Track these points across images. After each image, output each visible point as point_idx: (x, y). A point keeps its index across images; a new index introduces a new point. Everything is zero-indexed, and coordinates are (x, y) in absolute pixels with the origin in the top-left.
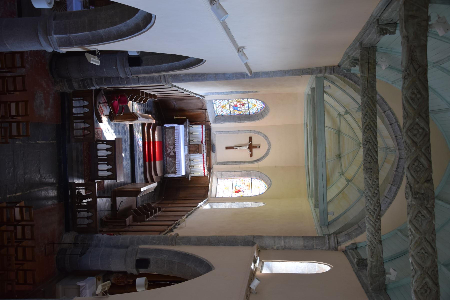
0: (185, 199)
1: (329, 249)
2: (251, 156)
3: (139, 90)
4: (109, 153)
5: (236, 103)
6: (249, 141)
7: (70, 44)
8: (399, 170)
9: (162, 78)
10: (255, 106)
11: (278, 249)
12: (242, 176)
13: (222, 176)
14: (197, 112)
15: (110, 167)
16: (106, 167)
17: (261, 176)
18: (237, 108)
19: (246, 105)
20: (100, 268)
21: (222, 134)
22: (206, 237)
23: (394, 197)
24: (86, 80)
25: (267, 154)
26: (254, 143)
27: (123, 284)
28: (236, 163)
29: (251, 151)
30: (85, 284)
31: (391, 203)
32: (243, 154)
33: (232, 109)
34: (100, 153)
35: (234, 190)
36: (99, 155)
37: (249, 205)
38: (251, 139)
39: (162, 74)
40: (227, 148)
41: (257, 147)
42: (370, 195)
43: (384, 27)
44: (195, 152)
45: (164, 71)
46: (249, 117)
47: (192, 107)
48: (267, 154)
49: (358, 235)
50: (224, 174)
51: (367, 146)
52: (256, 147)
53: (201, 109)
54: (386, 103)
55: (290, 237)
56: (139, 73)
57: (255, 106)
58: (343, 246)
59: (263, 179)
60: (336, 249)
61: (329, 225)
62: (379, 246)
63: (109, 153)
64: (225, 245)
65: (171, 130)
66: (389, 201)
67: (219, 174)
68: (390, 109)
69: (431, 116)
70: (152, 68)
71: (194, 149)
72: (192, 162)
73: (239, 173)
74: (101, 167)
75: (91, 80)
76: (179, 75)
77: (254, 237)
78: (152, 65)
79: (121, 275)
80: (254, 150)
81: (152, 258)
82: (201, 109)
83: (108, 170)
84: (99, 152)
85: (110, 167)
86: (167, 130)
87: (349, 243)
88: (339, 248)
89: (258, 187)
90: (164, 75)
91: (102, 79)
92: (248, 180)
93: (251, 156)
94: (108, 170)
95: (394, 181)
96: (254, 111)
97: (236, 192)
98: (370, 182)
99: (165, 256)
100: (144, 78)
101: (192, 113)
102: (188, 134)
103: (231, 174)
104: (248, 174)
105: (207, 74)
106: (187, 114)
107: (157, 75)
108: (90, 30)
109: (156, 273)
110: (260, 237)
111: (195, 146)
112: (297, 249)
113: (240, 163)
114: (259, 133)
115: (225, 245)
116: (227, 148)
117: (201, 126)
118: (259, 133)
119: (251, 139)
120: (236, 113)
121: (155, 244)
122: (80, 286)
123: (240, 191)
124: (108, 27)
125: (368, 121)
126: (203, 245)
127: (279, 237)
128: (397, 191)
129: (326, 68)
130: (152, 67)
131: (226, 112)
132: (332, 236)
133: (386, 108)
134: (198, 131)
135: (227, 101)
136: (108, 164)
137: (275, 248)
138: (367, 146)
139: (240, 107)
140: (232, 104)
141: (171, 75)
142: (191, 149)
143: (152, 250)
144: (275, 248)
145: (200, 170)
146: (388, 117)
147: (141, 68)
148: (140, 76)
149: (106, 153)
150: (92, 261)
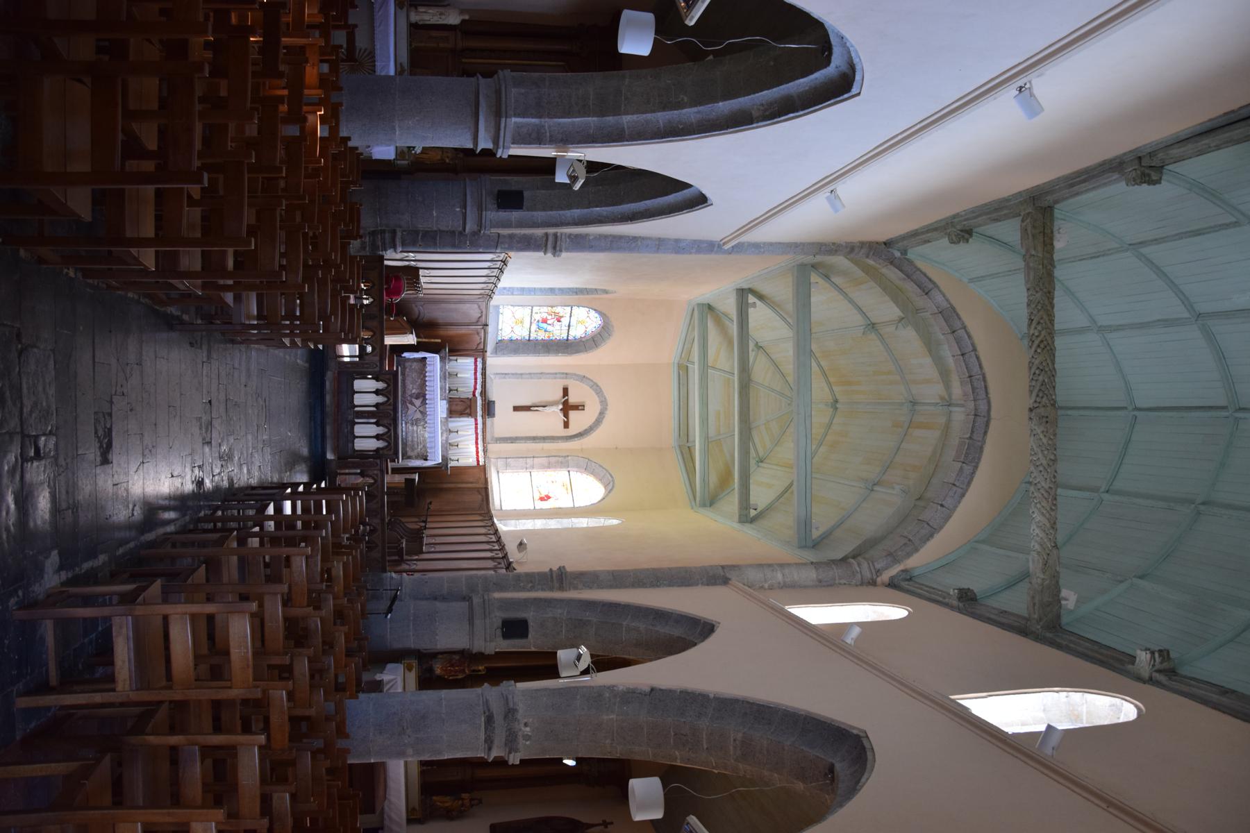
0: (440, 513)
1: (862, 584)
2: (566, 425)
3: (417, 269)
4: (381, 399)
5: (545, 315)
6: (561, 393)
7: (539, 140)
8: (975, 437)
9: (551, 239)
10: (584, 321)
11: (771, 588)
12: (549, 466)
13: (507, 466)
14: (463, 330)
15: (381, 430)
16: (373, 430)
17: (589, 466)
18: (544, 325)
19: (565, 321)
20: (411, 643)
21: (508, 379)
22: (628, 571)
23: (969, 483)
24: (383, 232)
25: (598, 422)
26: (573, 399)
27: (460, 677)
28: (534, 439)
29: (566, 415)
30: (392, 677)
31: (963, 495)
32: (550, 421)
33: (534, 327)
34: (358, 399)
35: (537, 496)
36: (356, 403)
37: (583, 523)
38: (566, 391)
39: (551, 231)
40: (516, 409)
41: (576, 407)
42: (1044, 462)
43: (1147, 171)
44: (462, 414)
45: (568, 224)
46: (566, 346)
47: (456, 317)
48: (598, 422)
49: (909, 555)
50: (508, 461)
51: (1041, 378)
52: (576, 407)
53: (476, 323)
54: (958, 315)
55: (789, 565)
56: (508, 225)
57: (582, 322)
58: (886, 577)
59: (593, 473)
60: (873, 583)
61: (816, 545)
62: (1055, 551)
63: (381, 399)
64: (669, 586)
65: (415, 365)
66: (960, 491)
67: (500, 463)
68: (965, 328)
69: (1059, 342)
70: (540, 215)
71: (459, 408)
72: (452, 435)
73: (544, 461)
74: (359, 430)
75: (394, 232)
76: (587, 235)
77: (723, 567)
78: (544, 210)
79: (457, 657)
80: (572, 414)
81: (529, 615)
82: (476, 323)
83: (378, 437)
84: (356, 396)
85: (381, 430)
86: (407, 364)
87: (895, 571)
88: (879, 580)
89: (589, 490)
90: (555, 235)
91: (416, 232)
92: (561, 475)
93: (566, 425)
94: (378, 437)
95: (967, 455)
96: (577, 332)
97: (542, 499)
98: (1045, 440)
99: (560, 611)
100: (511, 237)
101: (453, 331)
102: (446, 375)
103: (527, 462)
104: (561, 462)
105: (643, 238)
106: (442, 332)
107: (539, 232)
108: (602, 114)
109: (533, 649)
110: (734, 566)
111: (462, 400)
112: (805, 587)
113: (544, 439)
114: (583, 378)
115: (671, 585)
116: (516, 409)
117: (470, 361)
118: (583, 378)
119: (566, 391)
120: (541, 336)
121: (524, 589)
122: (381, 681)
123: (549, 497)
124: (654, 111)
125: (1043, 333)
126: (626, 587)
127: (770, 565)
128: (973, 473)
129: (862, 244)
130: (543, 213)
131: (521, 333)
132: (53, 679)
133: (958, 325)
134: (465, 366)
135: (528, 310)
136: (377, 424)
137: (766, 586)
138: (1041, 378)
139: (552, 325)
140: (537, 317)
141: (570, 236)
142: (454, 408)
143: (526, 600)
144: (766, 586)
145: (466, 454)
146: (958, 341)
147: (515, 215)
148: (505, 232)
149: (373, 399)
150: (397, 631)
